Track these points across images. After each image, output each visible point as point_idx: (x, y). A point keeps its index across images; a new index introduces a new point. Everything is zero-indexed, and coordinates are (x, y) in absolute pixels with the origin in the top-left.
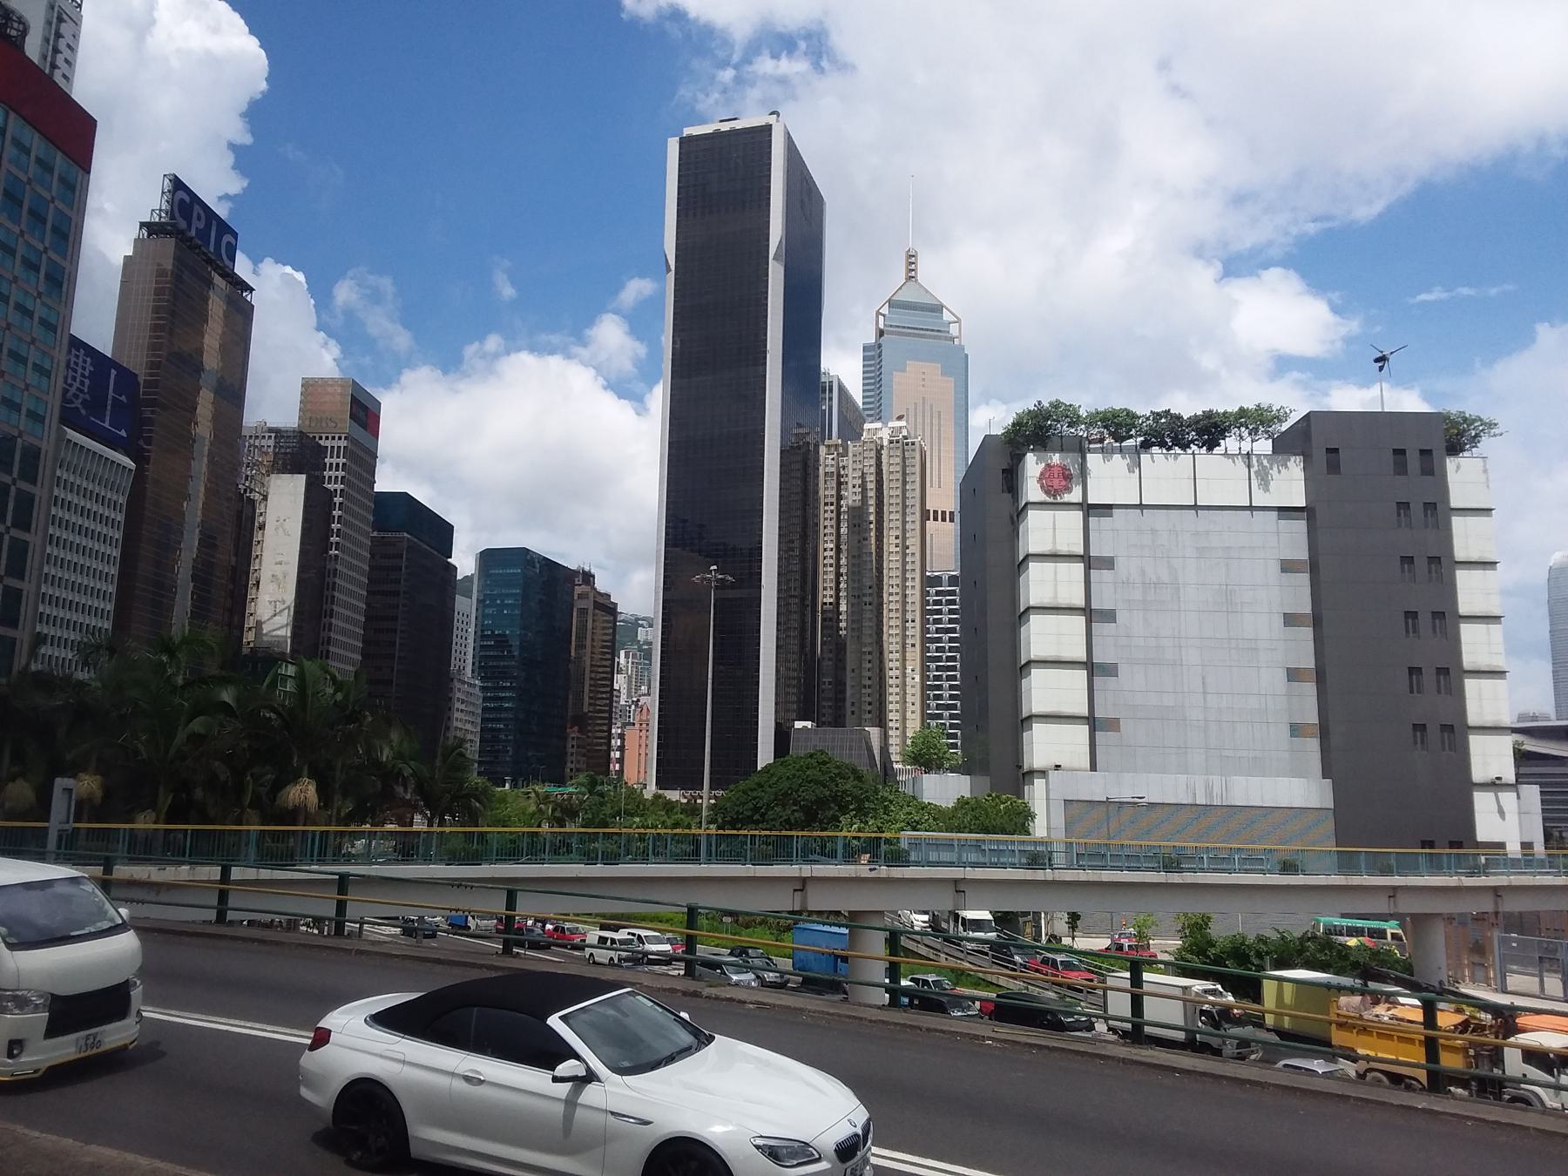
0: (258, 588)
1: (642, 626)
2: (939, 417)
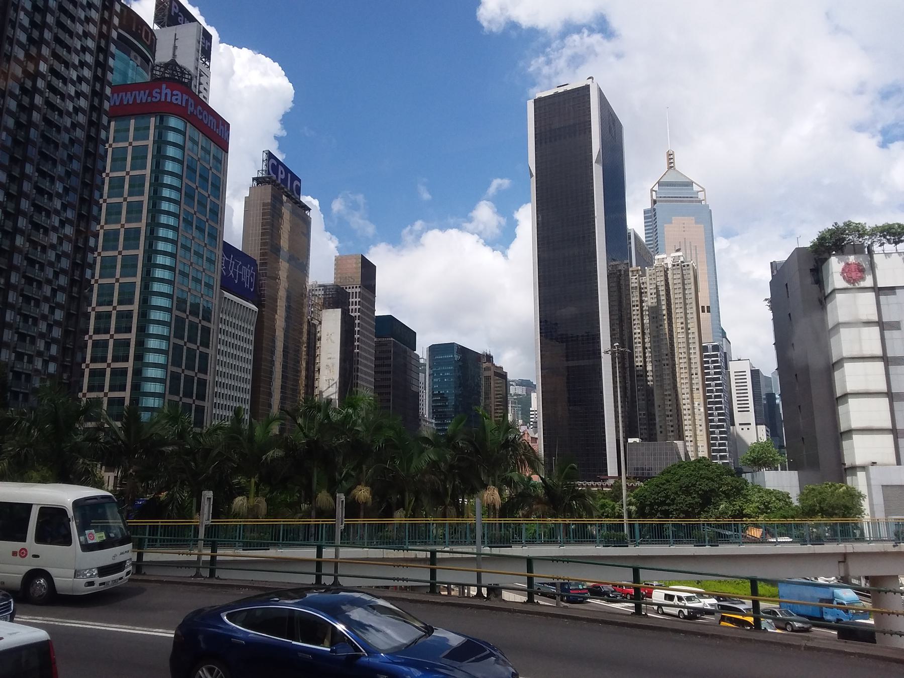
0: (319, 373)
1: (512, 385)
2: (696, 249)
